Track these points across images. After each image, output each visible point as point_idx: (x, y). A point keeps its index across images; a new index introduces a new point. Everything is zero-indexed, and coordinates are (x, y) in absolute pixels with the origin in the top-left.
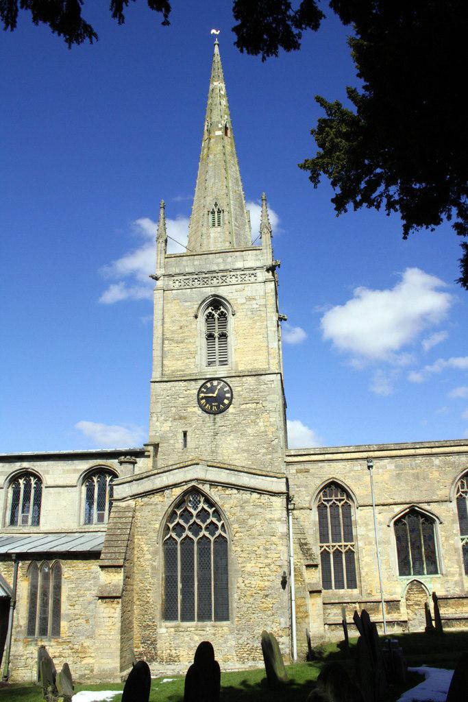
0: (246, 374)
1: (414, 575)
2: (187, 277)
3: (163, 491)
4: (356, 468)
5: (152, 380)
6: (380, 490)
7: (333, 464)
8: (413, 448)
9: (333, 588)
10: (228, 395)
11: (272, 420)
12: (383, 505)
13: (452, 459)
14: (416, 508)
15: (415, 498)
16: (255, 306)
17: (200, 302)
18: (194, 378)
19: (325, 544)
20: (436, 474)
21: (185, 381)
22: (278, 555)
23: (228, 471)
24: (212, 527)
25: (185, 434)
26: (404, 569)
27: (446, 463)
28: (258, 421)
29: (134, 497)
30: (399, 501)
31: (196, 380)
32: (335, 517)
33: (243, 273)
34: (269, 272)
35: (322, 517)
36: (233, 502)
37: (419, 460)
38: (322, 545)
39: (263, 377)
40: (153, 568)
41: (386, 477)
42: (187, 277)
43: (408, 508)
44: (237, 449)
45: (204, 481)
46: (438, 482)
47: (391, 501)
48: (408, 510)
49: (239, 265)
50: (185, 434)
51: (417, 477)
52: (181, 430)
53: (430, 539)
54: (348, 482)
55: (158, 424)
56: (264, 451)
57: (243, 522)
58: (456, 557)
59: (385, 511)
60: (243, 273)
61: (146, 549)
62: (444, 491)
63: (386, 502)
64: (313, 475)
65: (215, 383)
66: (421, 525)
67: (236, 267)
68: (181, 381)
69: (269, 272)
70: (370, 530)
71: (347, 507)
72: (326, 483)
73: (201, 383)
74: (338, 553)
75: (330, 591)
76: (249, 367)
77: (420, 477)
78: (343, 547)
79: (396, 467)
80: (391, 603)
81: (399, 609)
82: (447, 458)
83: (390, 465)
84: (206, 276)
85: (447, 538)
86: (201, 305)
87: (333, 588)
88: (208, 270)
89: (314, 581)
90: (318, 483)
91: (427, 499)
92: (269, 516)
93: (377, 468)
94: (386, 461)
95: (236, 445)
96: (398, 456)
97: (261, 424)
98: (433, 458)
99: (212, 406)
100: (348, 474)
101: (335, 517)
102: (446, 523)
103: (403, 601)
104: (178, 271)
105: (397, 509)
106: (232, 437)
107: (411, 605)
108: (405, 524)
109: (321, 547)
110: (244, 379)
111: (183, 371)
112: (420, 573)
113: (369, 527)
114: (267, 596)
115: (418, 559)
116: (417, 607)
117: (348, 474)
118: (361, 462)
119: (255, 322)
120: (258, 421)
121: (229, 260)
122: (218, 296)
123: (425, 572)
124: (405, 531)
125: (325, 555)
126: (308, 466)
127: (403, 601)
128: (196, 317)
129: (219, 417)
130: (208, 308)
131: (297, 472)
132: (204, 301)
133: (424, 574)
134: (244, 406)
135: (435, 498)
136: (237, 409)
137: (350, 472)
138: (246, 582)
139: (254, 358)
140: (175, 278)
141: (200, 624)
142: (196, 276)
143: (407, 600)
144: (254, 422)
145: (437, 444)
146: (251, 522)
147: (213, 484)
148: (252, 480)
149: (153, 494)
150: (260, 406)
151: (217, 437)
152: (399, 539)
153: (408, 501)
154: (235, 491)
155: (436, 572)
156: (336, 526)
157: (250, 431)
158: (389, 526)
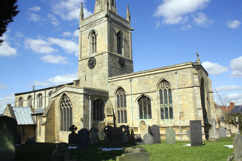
0: (99, 54)
1: (148, 118)
2: (87, 26)
3: (59, 95)
4: (127, 82)
5: (79, 61)
6: (134, 89)
7: (120, 81)
8: (144, 73)
9: (121, 123)
10: (95, 62)
11: (105, 68)
12: (134, 94)
13: (157, 75)
14: (144, 95)
15: (144, 91)
16: (103, 31)
17: (89, 34)
18: (87, 58)
19: (118, 108)
20: (151, 82)
21: (85, 59)
22: (81, 113)
23: (72, 88)
24: (69, 104)
25: (85, 76)
26: (141, 117)
27: (155, 77)
28: (102, 69)
29: (55, 97)
30: (139, 93)
31: (88, 59)
32: (122, 99)
33: (100, 20)
34: (106, 18)
35: (118, 99)
36: (73, 97)
37: (146, 77)
38: (161, 105)
39: (103, 54)
40: (58, 117)
41: (135, 84)
42: (87, 26)
43: (142, 95)
44: (97, 79)
45: (67, 91)
46: (152, 85)
47: (137, 93)
48: (142, 96)
49: (99, 18)
50: (85, 76)
51: (145, 83)
52: (84, 75)
53: (150, 106)
54: (124, 87)
55: (80, 74)
56: (103, 79)
57: (74, 103)
58: (157, 113)
59: (135, 96)
60: (100, 20)
61: (57, 111)
62: (154, 88)
63: (135, 93)
64: (115, 86)
65: (92, 59)
66: (147, 101)
67: (98, 19)
68: (84, 60)
69: (106, 18)
70: (130, 103)
71: (125, 96)
72: (118, 88)
73: (89, 59)
74: (122, 111)
75: (120, 124)
76: (101, 52)
77: (146, 83)
78: (120, 109)
79: (139, 80)
80: (136, 128)
81: (138, 130)
82: (156, 75)
83: (136, 80)
84: (91, 24)
85: (154, 105)
86: (89, 34)
87: (121, 123)
88: (91, 22)
89: (111, 120)
90: (116, 88)
91: (148, 91)
92: (80, 101)
93: (133, 81)
94: (136, 78)
95: (96, 78)
96: (139, 76)
97: (103, 70)
98: (151, 76)
99: (91, 66)
100: (124, 84)
101: (122, 99)
102: (154, 100)
103: (139, 128)
104: (84, 25)
105: (138, 95)
106: (96, 75)
107: (142, 129)
108: (142, 101)
109: (161, 106)
110: (99, 56)
111: (86, 56)
112: (146, 118)
113: (130, 102)
114: (79, 125)
115: (145, 113)
116: (143, 130)
117: (124, 84)
118: (128, 79)
119: (103, 36)
120: (102, 69)
121: (97, 17)
122: (93, 30)
123: (148, 118)
124: (142, 103)
125: (118, 111)
126: (114, 83)
127: (139, 128)
128: (88, 38)
129: (93, 69)
130: (92, 34)
131: (111, 85)
132: (90, 33)
133: (147, 119)
134: (99, 65)
135: (151, 91)
136: (97, 66)
137: (125, 83)
138: (75, 120)
139: (102, 48)
140: (84, 27)
141: (67, 132)
142: (89, 25)
143: (140, 127)
144: (101, 70)
145: (152, 70)
146: (76, 103)
147: (69, 92)
148: (58, 92)
149: (58, 96)
150: (102, 64)
151: (92, 76)
152: (140, 106)
153: (142, 92)
154: (73, 94)
155: (151, 118)
156: (122, 102)
157: (100, 73)
158: (135, 102)
